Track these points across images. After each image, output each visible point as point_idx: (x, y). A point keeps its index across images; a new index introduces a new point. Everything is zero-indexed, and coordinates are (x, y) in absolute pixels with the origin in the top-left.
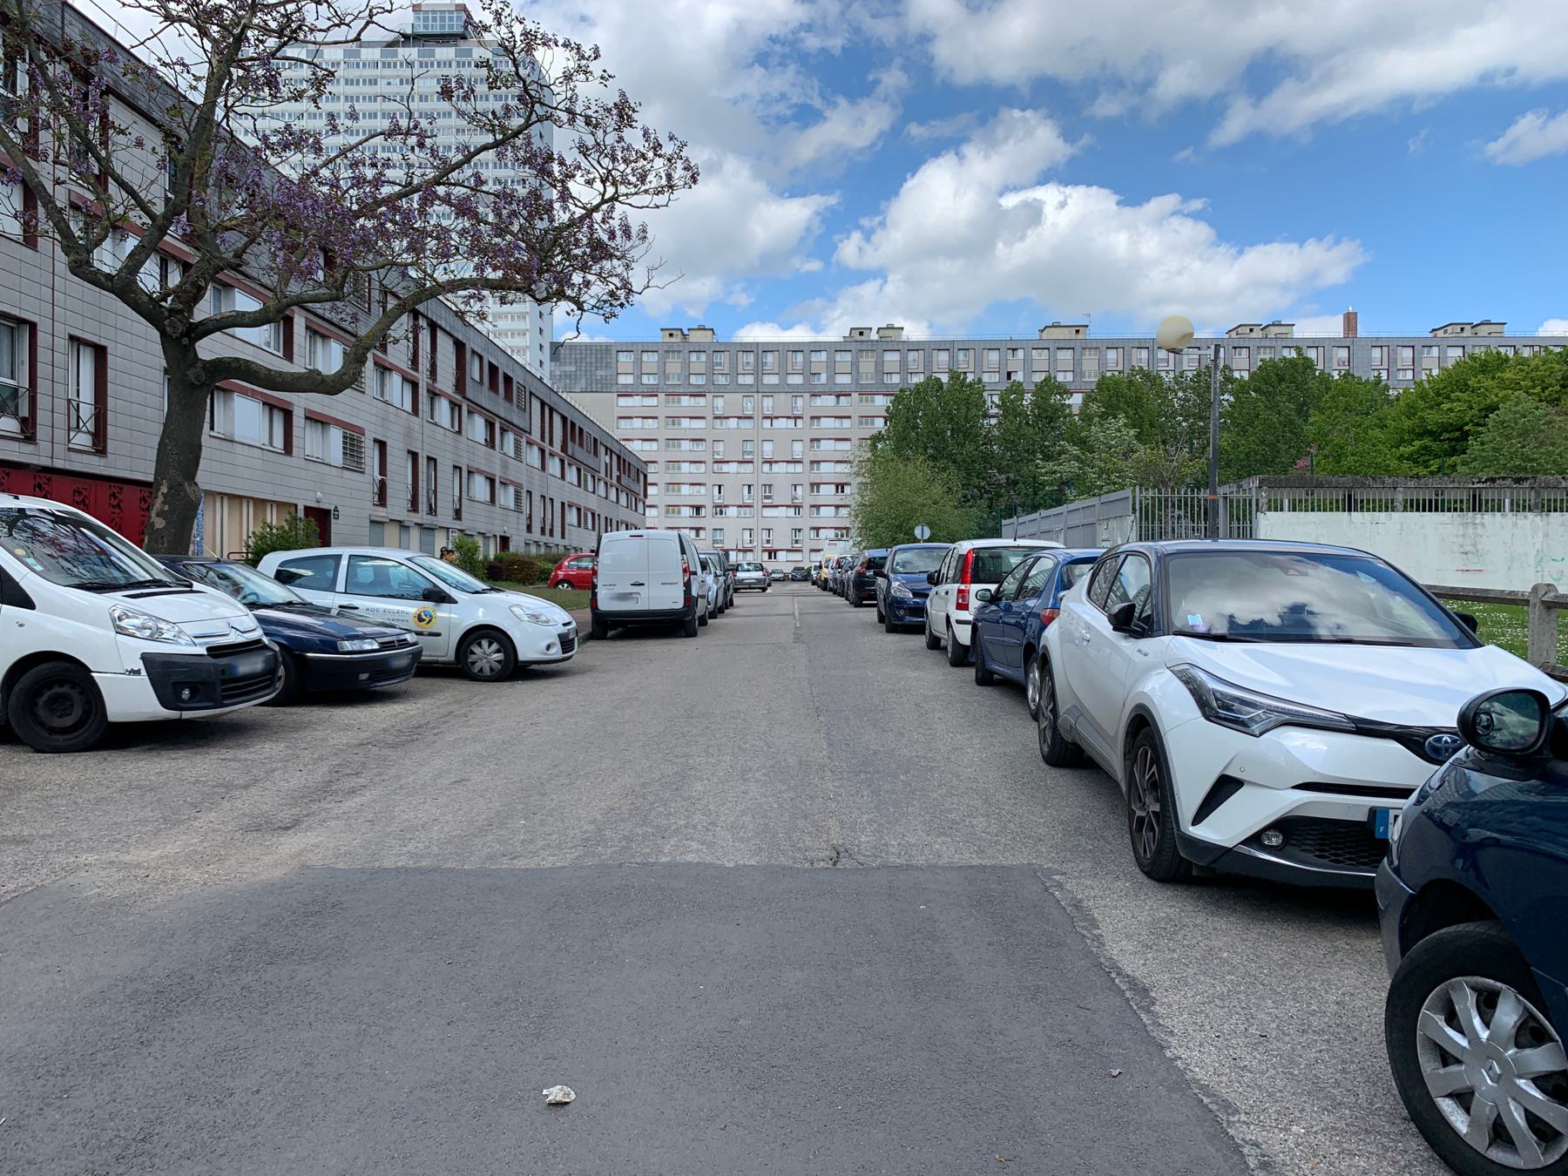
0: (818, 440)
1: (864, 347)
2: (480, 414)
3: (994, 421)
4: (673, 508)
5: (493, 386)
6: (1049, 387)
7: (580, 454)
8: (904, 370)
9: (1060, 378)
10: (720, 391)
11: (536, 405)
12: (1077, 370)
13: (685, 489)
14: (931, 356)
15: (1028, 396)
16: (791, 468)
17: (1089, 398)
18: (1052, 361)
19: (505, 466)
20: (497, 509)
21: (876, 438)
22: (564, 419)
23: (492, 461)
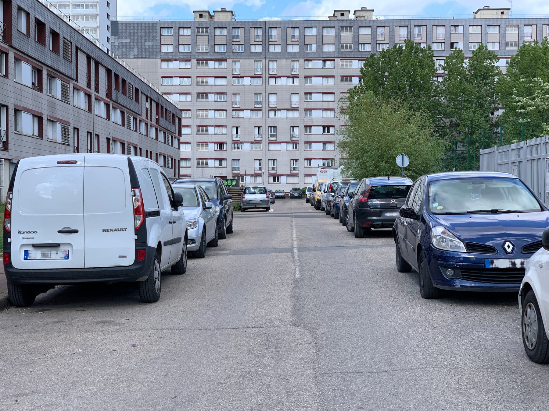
0: (310, 93)
1: (344, 24)
2: (27, 61)
3: (440, 79)
4: (202, 145)
5: (41, 40)
6: (482, 54)
7: (123, 100)
8: (374, 41)
9: (490, 47)
10: (237, 57)
11: (82, 59)
12: (502, 42)
13: (211, 130)
14: (394, 31)
15: (466, 61)
16: (290, 114)
17: (514, 62)
18: (484, 34)
19: (52, 106)
20: (44, 142)
21: (352, 93)
22: (109, 71)
23: (41, 102)
